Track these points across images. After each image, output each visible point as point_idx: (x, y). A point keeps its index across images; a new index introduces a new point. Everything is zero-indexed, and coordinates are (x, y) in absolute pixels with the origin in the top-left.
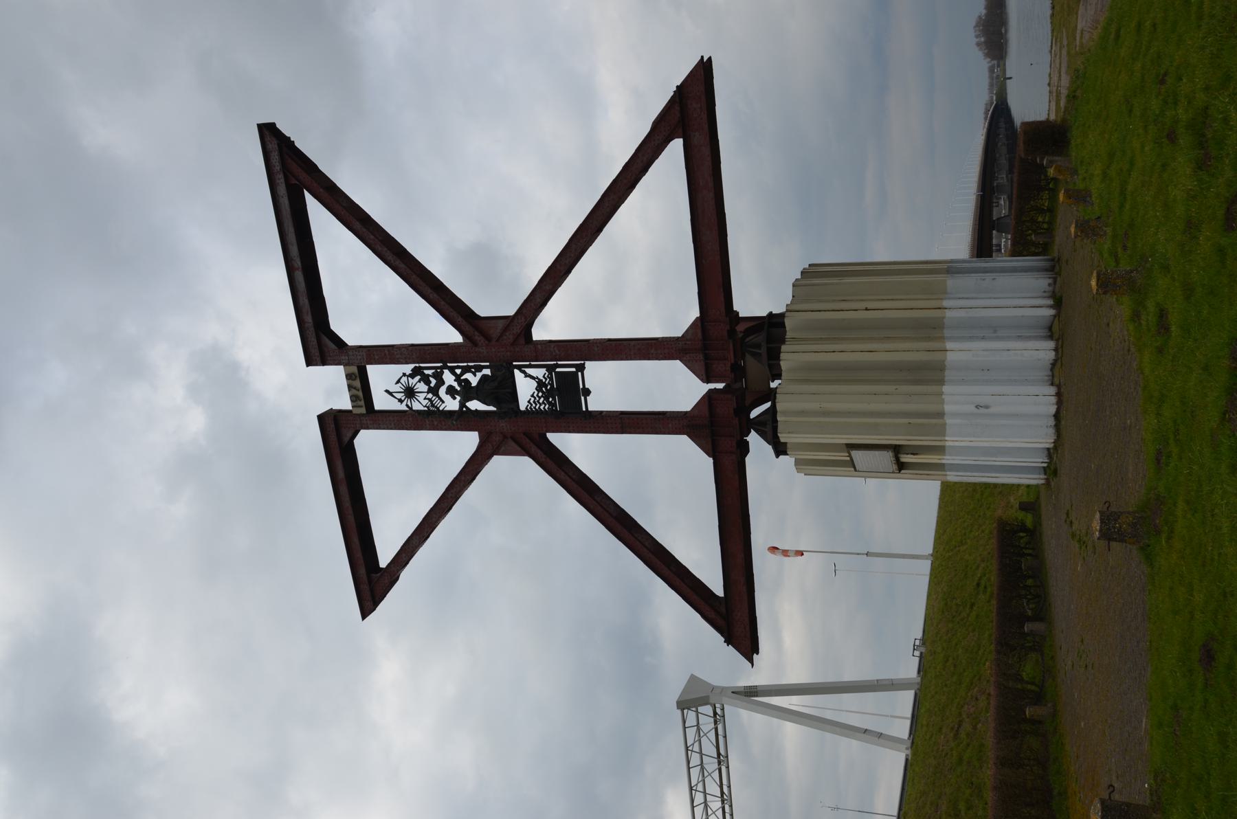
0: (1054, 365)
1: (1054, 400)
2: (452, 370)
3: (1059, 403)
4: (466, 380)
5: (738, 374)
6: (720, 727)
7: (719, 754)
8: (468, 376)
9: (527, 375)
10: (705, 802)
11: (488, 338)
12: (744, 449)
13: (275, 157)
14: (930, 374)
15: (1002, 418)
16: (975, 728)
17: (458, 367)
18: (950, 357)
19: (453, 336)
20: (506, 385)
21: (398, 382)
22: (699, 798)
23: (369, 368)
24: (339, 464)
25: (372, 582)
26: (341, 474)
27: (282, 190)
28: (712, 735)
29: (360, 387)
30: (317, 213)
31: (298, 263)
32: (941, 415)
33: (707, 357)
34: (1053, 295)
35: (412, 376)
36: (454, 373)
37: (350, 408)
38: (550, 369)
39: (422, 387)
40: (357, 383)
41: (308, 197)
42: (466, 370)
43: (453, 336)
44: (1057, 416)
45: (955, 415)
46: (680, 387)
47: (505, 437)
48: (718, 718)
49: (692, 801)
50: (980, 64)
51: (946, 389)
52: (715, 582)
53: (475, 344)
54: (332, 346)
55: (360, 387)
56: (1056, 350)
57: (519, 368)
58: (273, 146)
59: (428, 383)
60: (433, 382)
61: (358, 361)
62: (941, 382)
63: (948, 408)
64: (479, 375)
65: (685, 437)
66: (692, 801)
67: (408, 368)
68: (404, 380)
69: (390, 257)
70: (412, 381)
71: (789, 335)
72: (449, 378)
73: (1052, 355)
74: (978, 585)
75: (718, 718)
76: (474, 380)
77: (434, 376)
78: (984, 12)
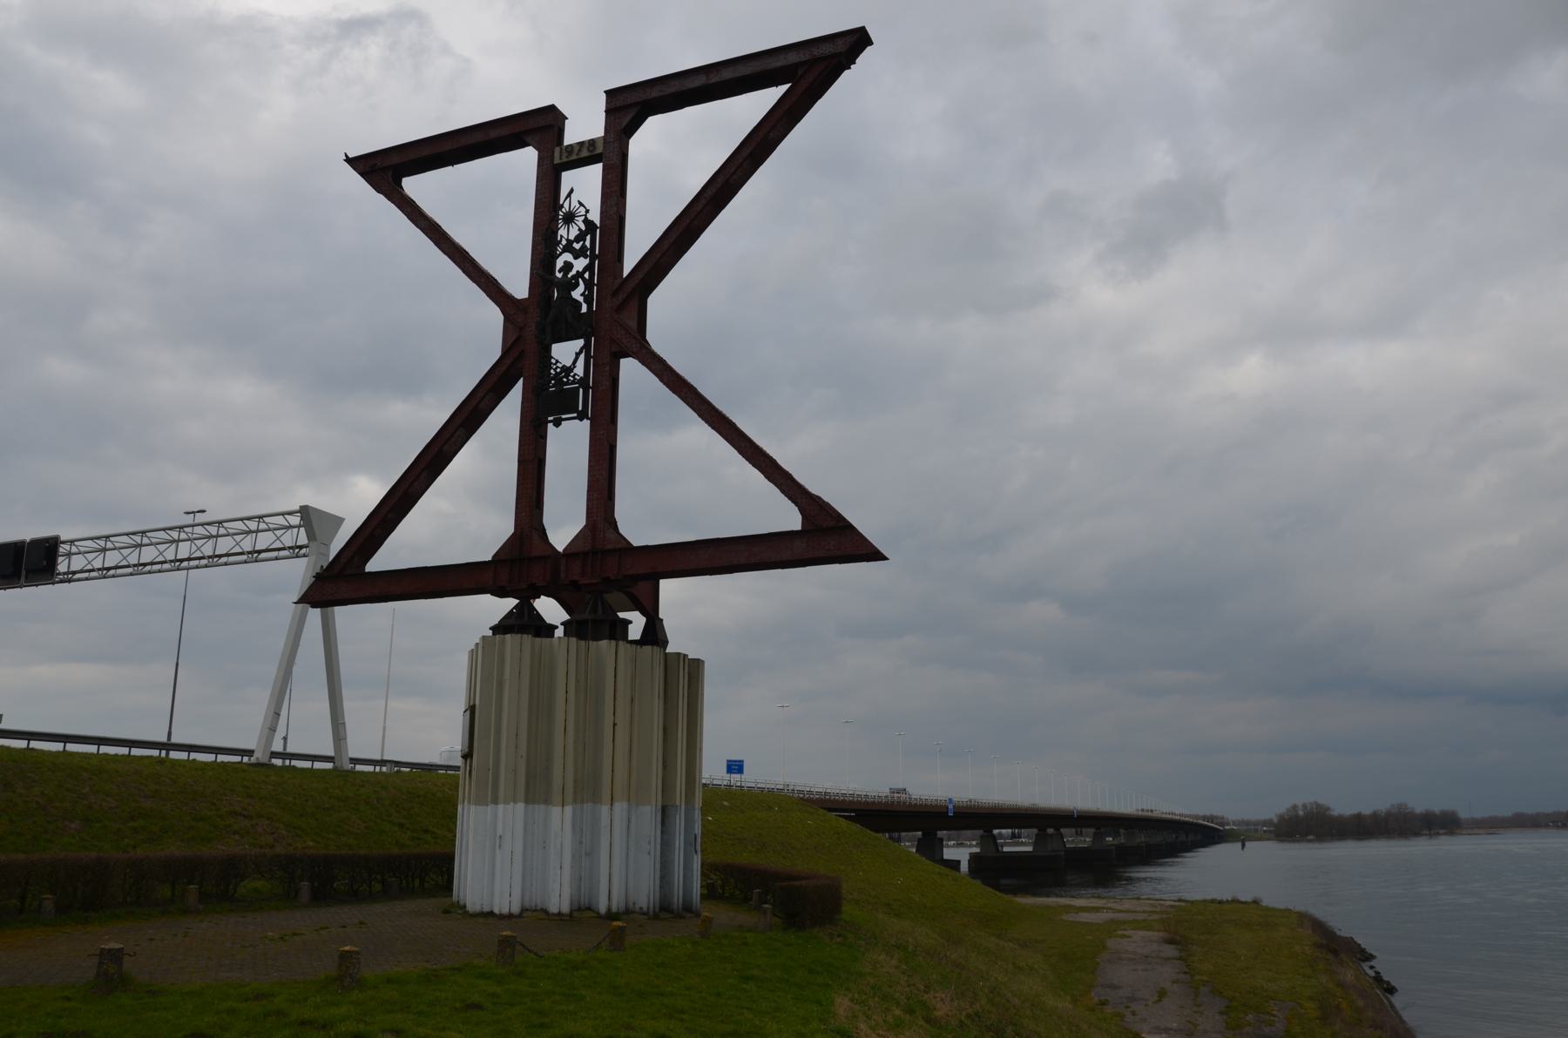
0: (545, 911)
1: (505, 911)
2: (589, 268)
3: (502, 917)
4: (577, 285)
5: (590, 583)
6: (286, 553)
7: (259, 552)
8: (581, 288)
9: (578, 355)
10: (251, 532)
11: (619, 309)
12: (501, 593)
13: (827, 49)
14: (536, 790)
15: (503, 860)
16: (235, 833)
17: (592, 275)
18: (556, 811)
19: (631, 258)
20: (575, 327)
21: (581, 204)
22: (253, 525)
23: (599, 166)
24: (504, 131)
25: (386, 169)
26: (494, 134)
27: (793, 58)
28: (278, 545)
29: (585, 155)
30: (765, 99)
31: (714, 79)
32: (495, 801)
33: (586, 554)
34: (628, 912)
35: (586, 221)
36: (585, 270)
37: (566, 143)
38: (583, 382)
39: (574, 232)
40: (585, 153)
41: (784, 88)
42: (589, 285)
43: (631, 258)
44: (491, 914)
45: (495, 816)
46: (564, 525)
47: (521, 329)
48: (296, 550)
49: (249, 519)
50: (1272, 808)
51: (521, 806)
52: (380, 562)
53: (615, 294)
54: (625, 121)
55: (585, 155)
56: (559, 914)
57: (586, 347)
58: (840, 47)
59: (577, 239)
60: (577, 246)
61: (611, 155)
62: (528, 800)
63: (501, 807)
64: (581, 299)
65: (512, 531)
66: (249, 519)
67: (595, 217)
68: (582, 211)
69: (709, 193)
70: (580, 221)
71: (593, 644)
72: (580, 264)
73: (554, 909)
74: (426, 831)
75: (296, 550)
76: (577, 294)
77: (584, 246)
78: (1335, 813)
